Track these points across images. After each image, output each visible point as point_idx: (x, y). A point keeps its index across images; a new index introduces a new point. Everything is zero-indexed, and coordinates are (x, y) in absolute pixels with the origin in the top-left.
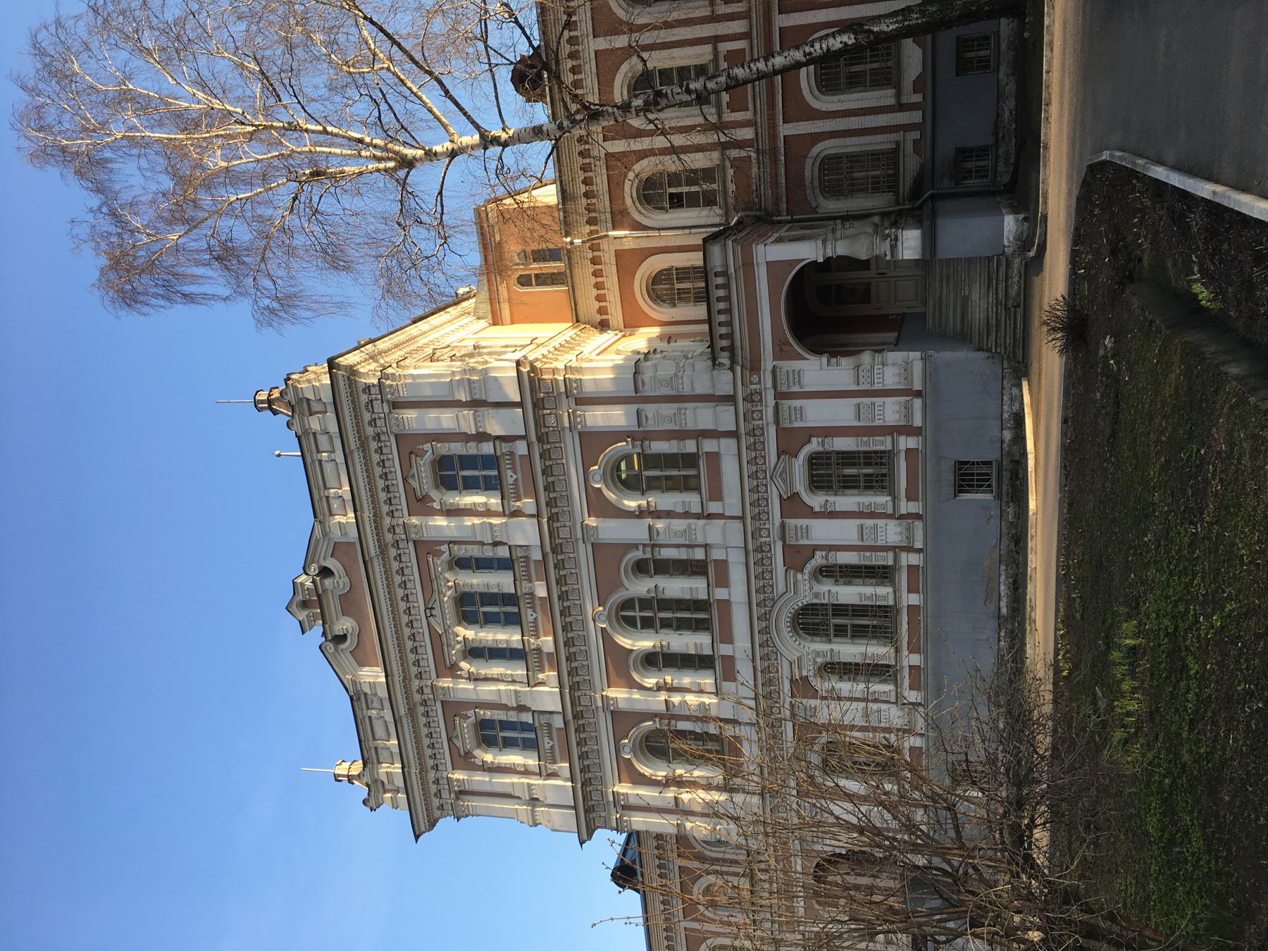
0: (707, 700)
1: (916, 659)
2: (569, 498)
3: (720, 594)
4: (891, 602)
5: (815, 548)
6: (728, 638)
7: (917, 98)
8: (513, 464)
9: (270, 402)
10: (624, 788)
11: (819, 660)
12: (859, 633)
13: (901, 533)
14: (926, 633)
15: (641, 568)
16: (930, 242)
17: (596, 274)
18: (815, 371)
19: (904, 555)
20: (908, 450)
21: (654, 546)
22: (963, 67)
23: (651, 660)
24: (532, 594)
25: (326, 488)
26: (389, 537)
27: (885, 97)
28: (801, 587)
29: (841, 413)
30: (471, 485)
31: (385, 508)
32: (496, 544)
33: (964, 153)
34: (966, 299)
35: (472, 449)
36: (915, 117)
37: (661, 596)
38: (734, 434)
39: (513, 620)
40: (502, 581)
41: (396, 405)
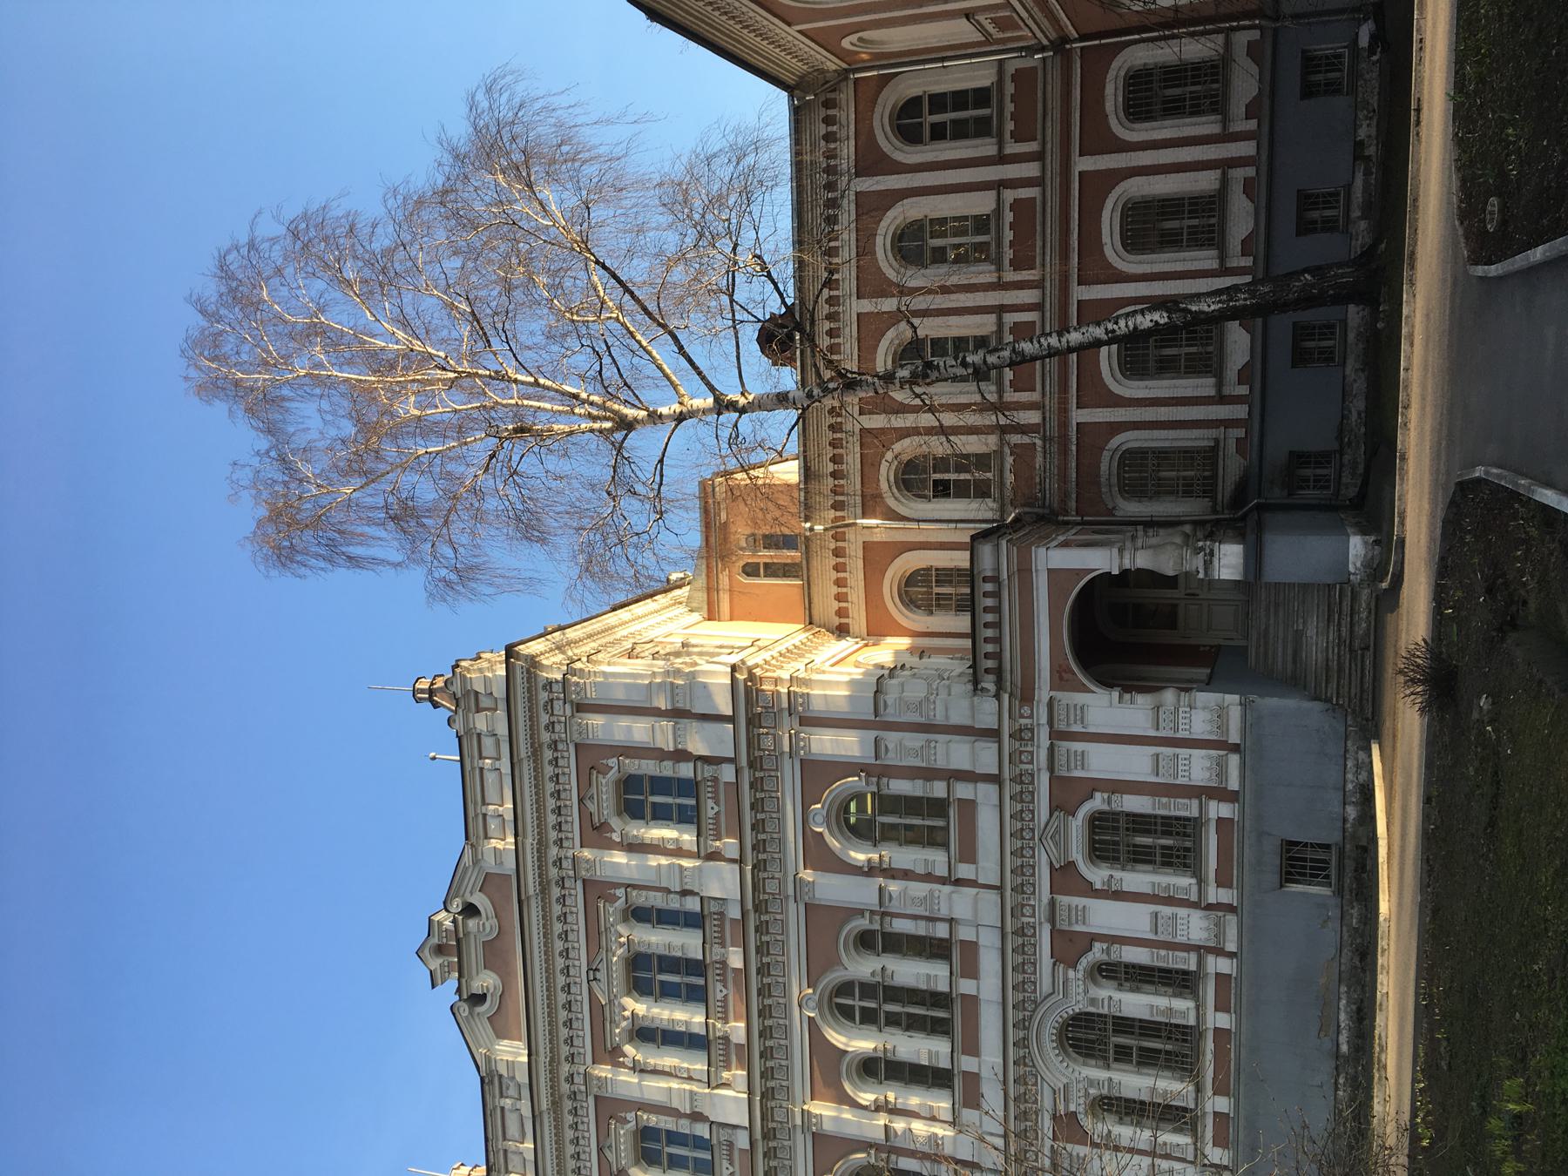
1: (1223, 1104)
2: (782, 842)
3: (966, 986)
5: (1094, 938)
6: (973, 1048)
7: (1243, 390)
8: (716, 792)
9: (431, 692)
11: (1092, 1091)
12: (1148, 1059)
13: (1208, 929)
15: (865, 941)
16: (1255, 560)
18: (1102, 708)
19: (1211, 959)
20: (1219, 820)
21: (884, 914)
22: (1300, 358)
23: (870, 1068)
24: (724, 963)
25: (484, 803)
26: (553, 872)
27: (1203, 386)
28: (1073, 989)
29: (1134, 764)
30: (661, 815)
31: (553, 835)
32: (685, 893)
33: (1299, 458)
34: (1299, 636)
35: (667, 769)
36: (1240, 411)
38: (996, 779)
39: (696, 995)
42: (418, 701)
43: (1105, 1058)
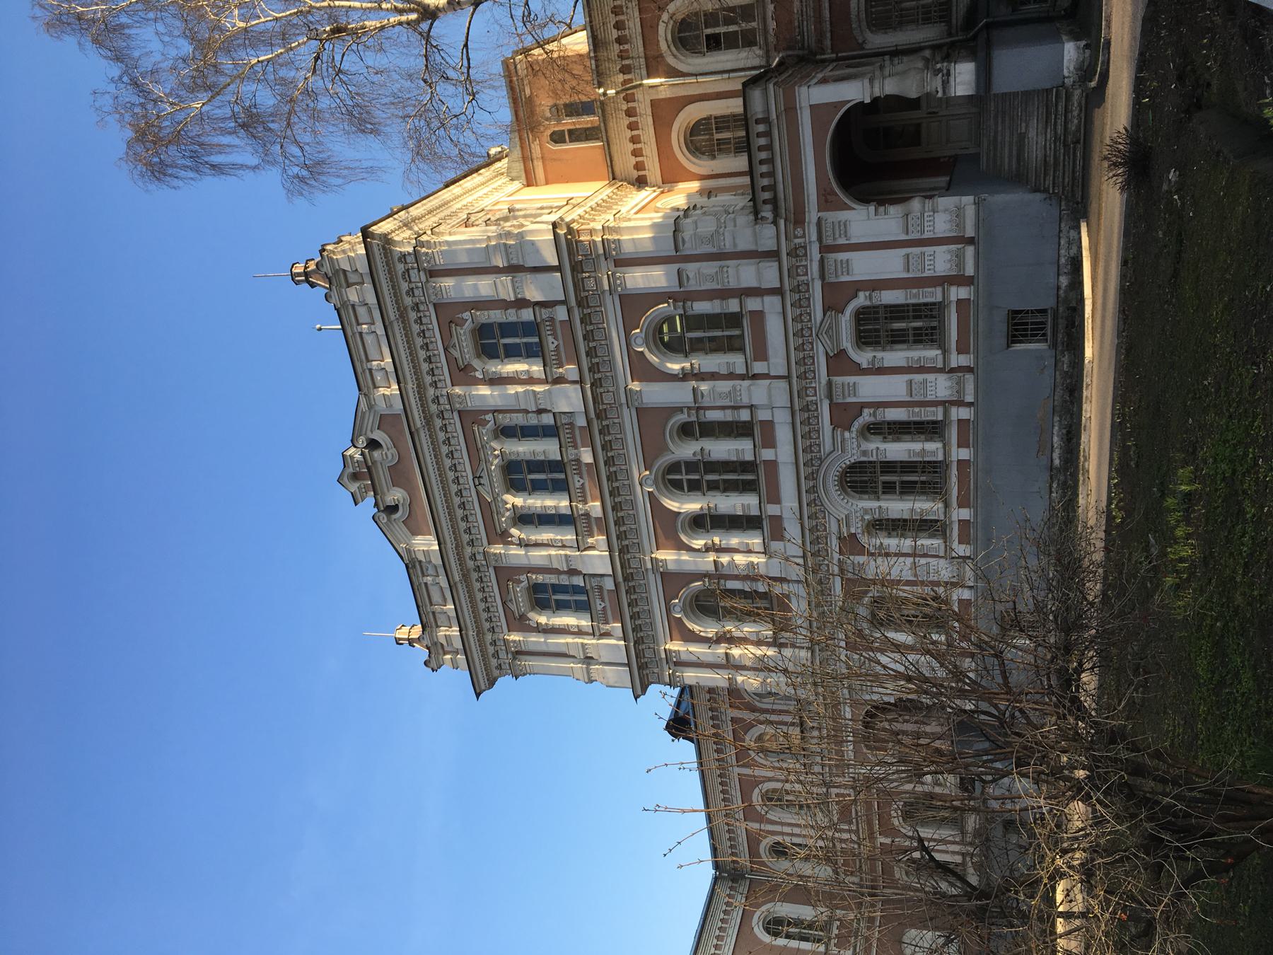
0: (755, 559)
1: (965, 514)
2: (611, 363)
3: (767, 454)
4: (940, 458)
5: (863, 405)
6: (775, 498)
10: (675, 646)
14: (976, 488)
15: (686, 431)
16: (984, 76)
17: (632, 127)
18: (862, 221)
19: (954, 410)
23: (698, 522)
24: (578, 461)
30: (512, 353)
31: (428, 379)
32: (540, 411)
34: (1022, 137)
37: (707, 459)
38: (778, 292)
39: (560, 487)
40: (548, 449)
41: (433, 273)
42: (297, 283)
43: (876, 493)
